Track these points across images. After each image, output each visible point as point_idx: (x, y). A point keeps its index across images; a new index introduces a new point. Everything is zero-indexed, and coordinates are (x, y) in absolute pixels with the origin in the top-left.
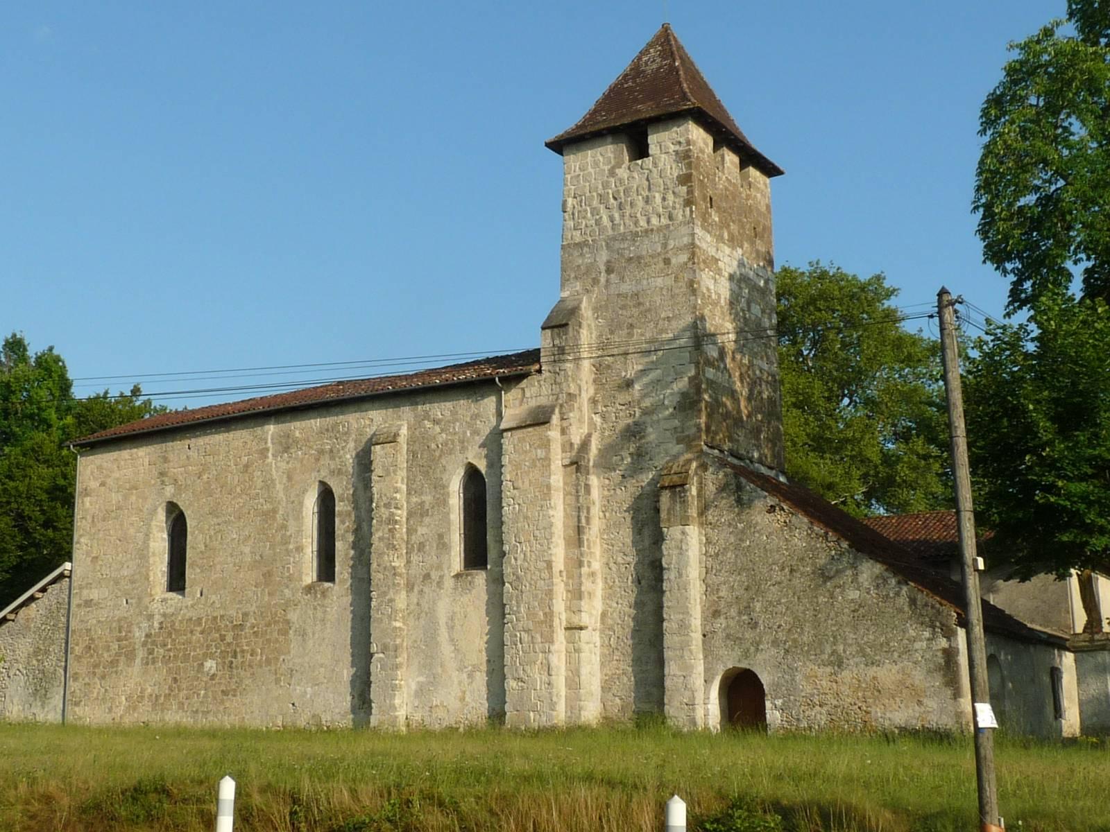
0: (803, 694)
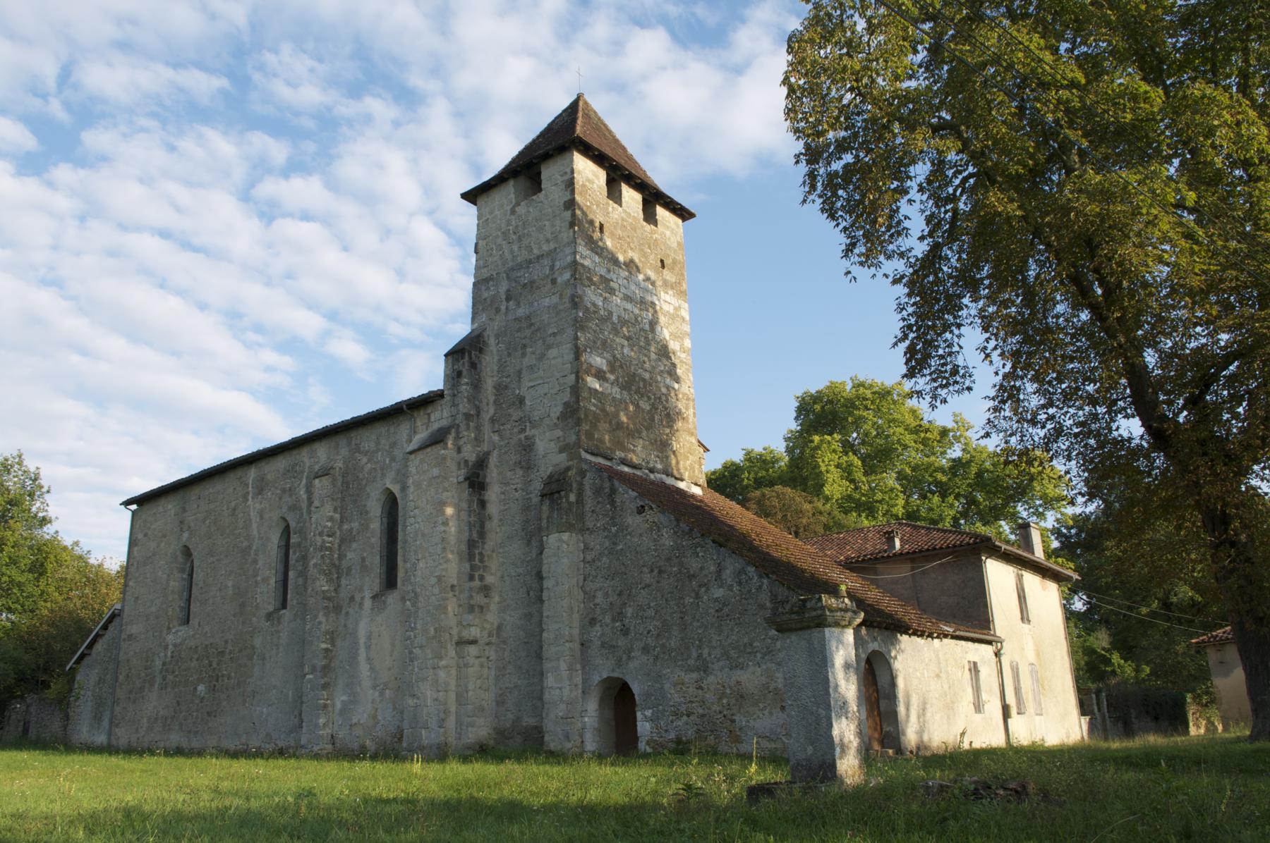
0: (671, 703)
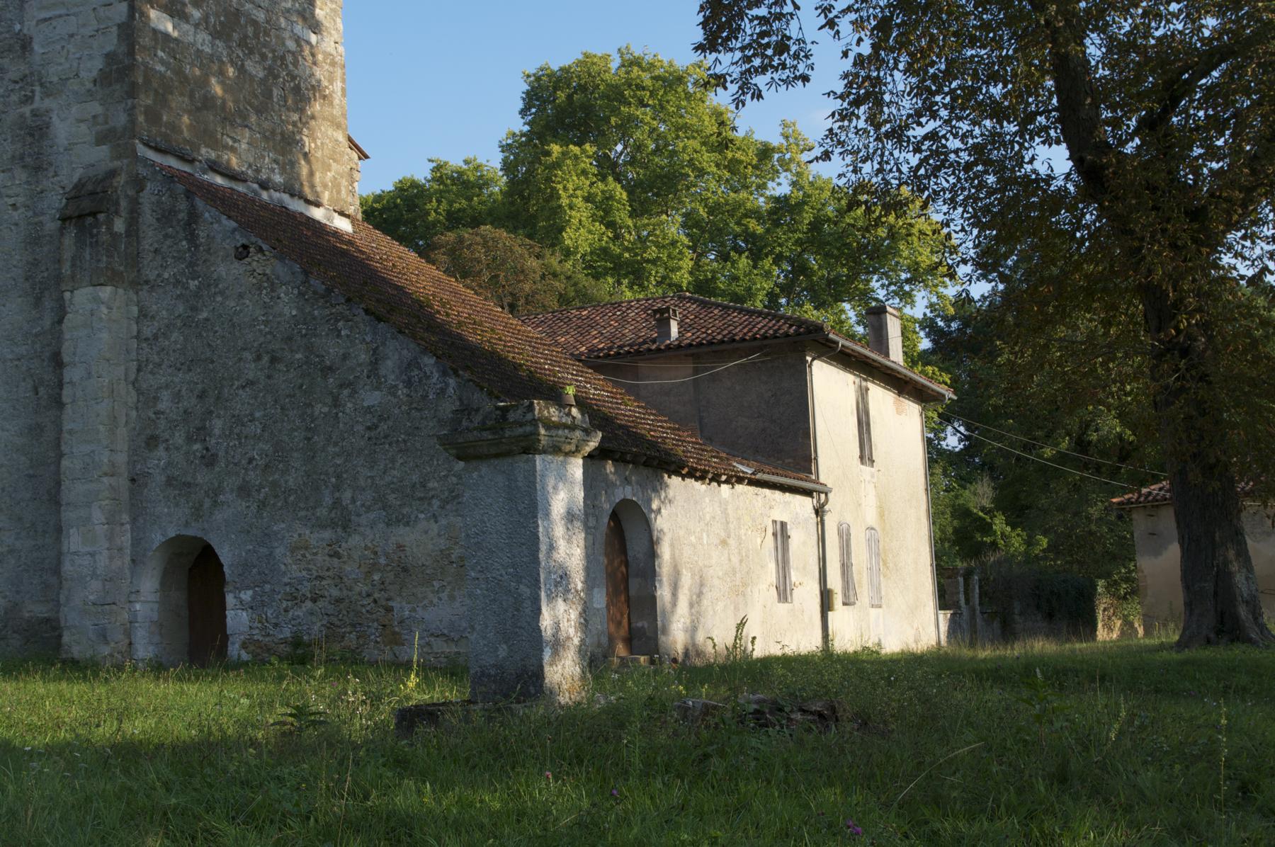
0: (286, 580)
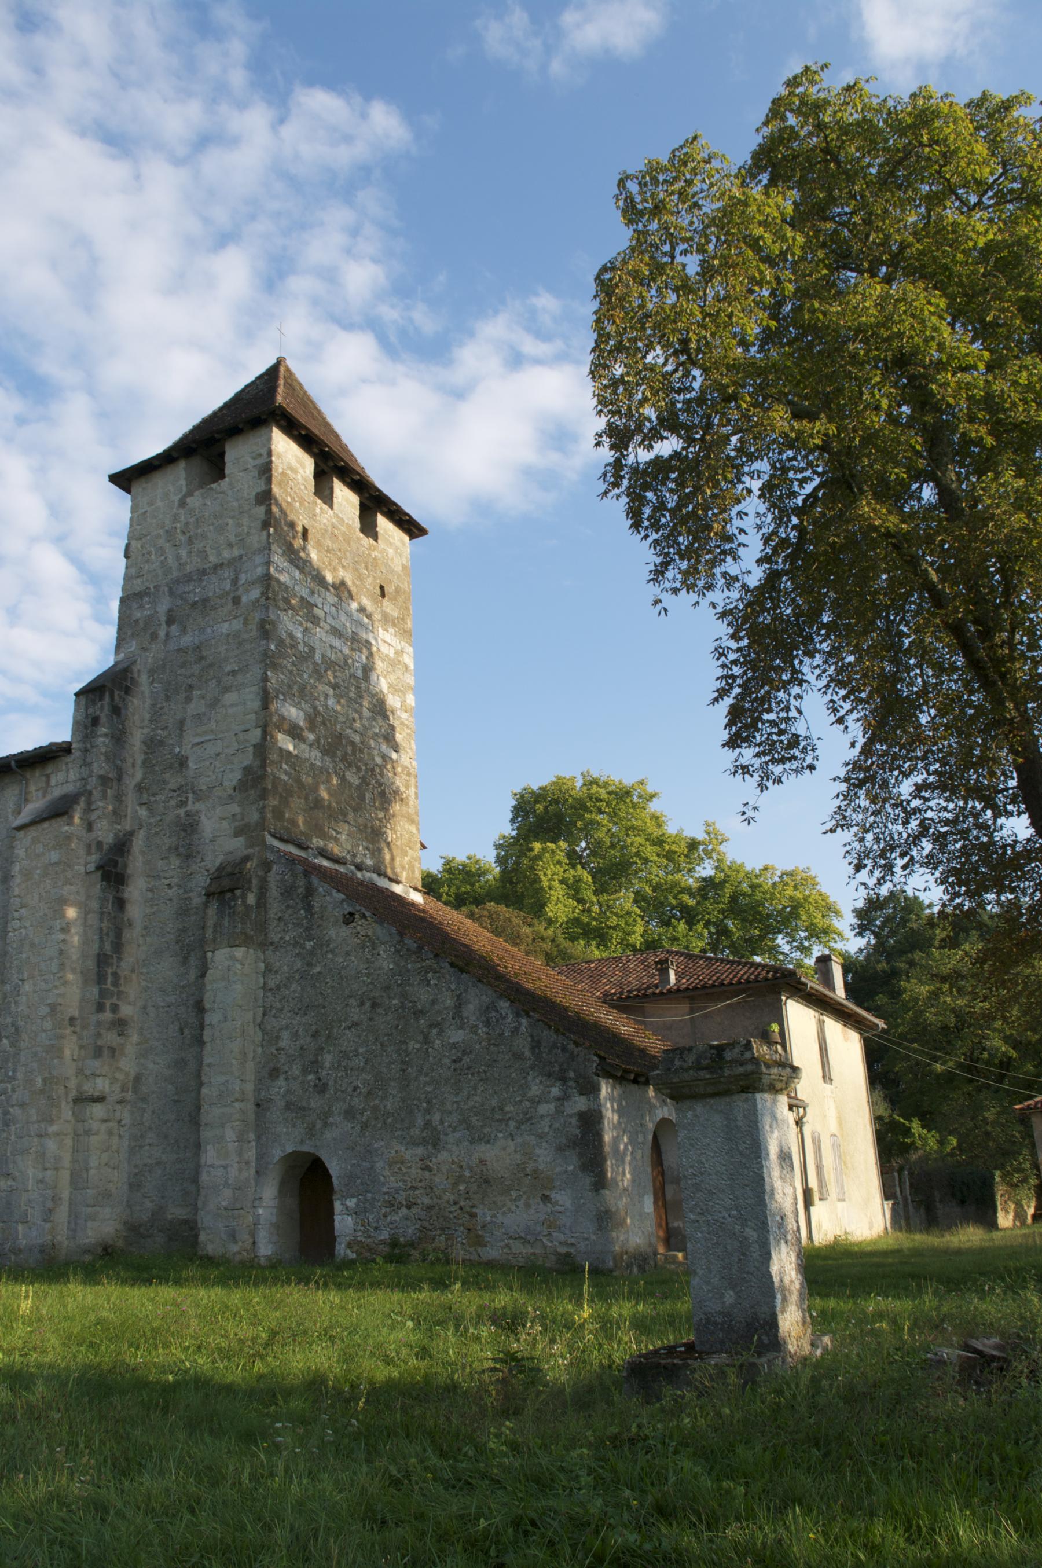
0: (385, 1189)
